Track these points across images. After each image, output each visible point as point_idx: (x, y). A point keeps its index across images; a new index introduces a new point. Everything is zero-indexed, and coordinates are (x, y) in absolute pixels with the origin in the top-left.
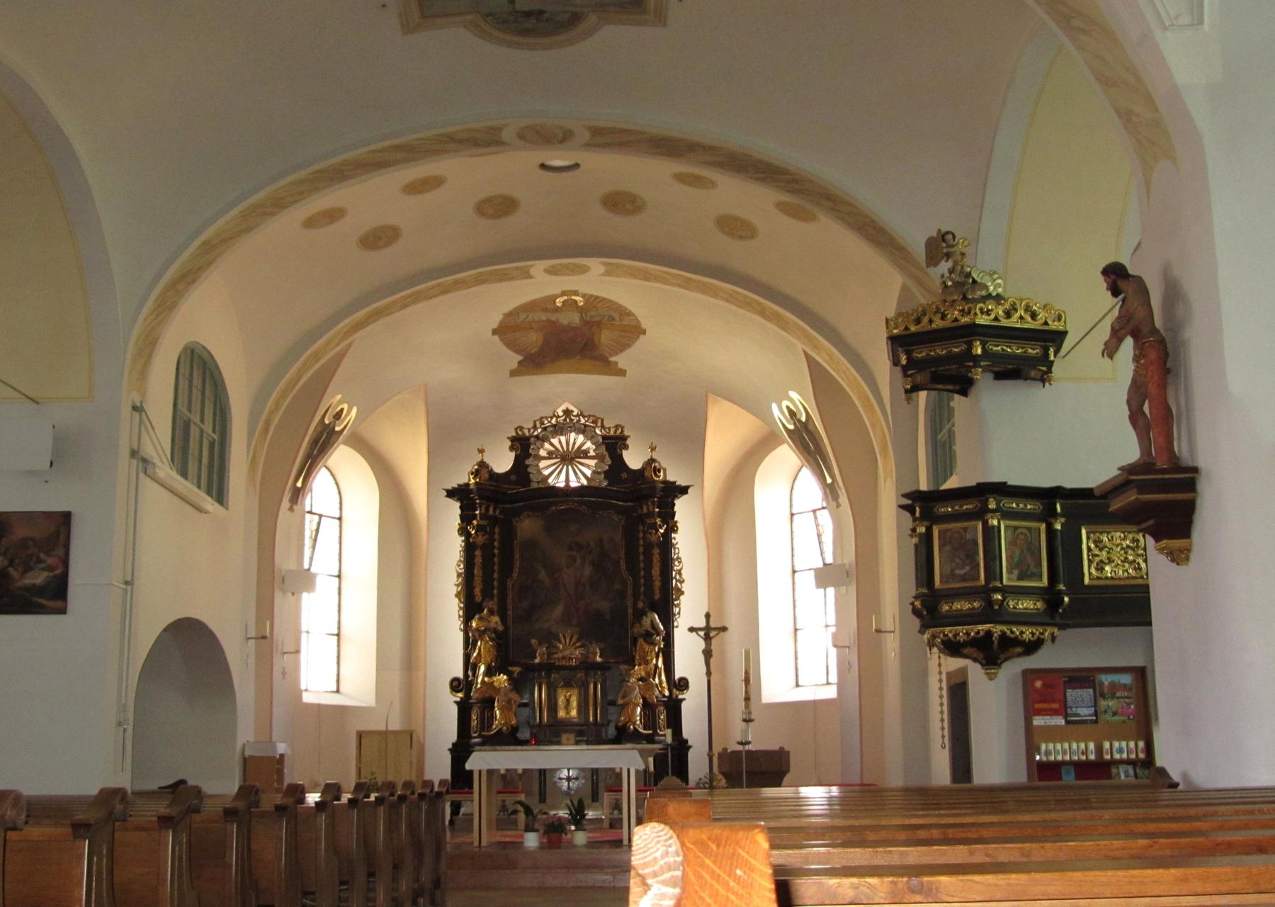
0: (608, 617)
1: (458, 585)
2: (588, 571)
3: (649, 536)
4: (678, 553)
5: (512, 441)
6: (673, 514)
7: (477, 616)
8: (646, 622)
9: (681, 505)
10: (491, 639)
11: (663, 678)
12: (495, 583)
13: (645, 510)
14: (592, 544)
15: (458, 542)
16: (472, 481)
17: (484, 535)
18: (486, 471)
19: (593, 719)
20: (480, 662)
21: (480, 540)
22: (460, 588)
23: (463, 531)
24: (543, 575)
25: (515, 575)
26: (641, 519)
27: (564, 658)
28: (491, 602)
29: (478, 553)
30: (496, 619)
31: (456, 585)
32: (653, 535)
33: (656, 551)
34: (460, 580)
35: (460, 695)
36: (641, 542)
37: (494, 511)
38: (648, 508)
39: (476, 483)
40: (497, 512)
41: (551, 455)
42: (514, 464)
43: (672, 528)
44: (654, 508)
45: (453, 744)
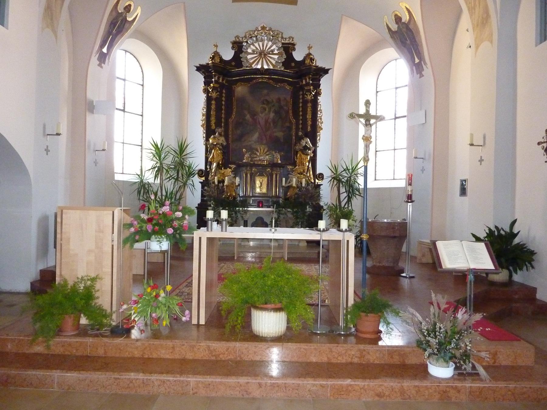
0: (282, 141)
1: (202, 121)
2: (272, 115)
3: (306, 96)
4: (320, 107)
5: (233, 44)
6: (319, 85)
7: (212, 136)
8: (303, 143)
9: (324, 81)
10: (220, 149)
11: (311, 173)
12: (223, 120)
13: (304, 82)
14: (274, 100)
15: (203, 97)
16: (211, 62)
17: (216, 93)
18: (218, 56)
19: (275, 194)
20: (213, 161)
21: (214, 95)
22: (204, 122)
23: (206, 91)
24: (248, 117)
25: (233, 117)
26: (302, 88)
27: (260, 160)
28: (220, 129)
29: (213, 102)
30: (222, 139)
31: (201, 120)
32: (309, 96)
33: (309, 105)
34: (204, 117)
35: (203, 178)
36: (301, 101)
37: (223, 80)
38: (306, 81)
39: (212, 63)
40: (224, 82)
41: (253, 52)
42: (232, 58)
43: (318, 94)
44: (309, 81)
45: (199, 204)
